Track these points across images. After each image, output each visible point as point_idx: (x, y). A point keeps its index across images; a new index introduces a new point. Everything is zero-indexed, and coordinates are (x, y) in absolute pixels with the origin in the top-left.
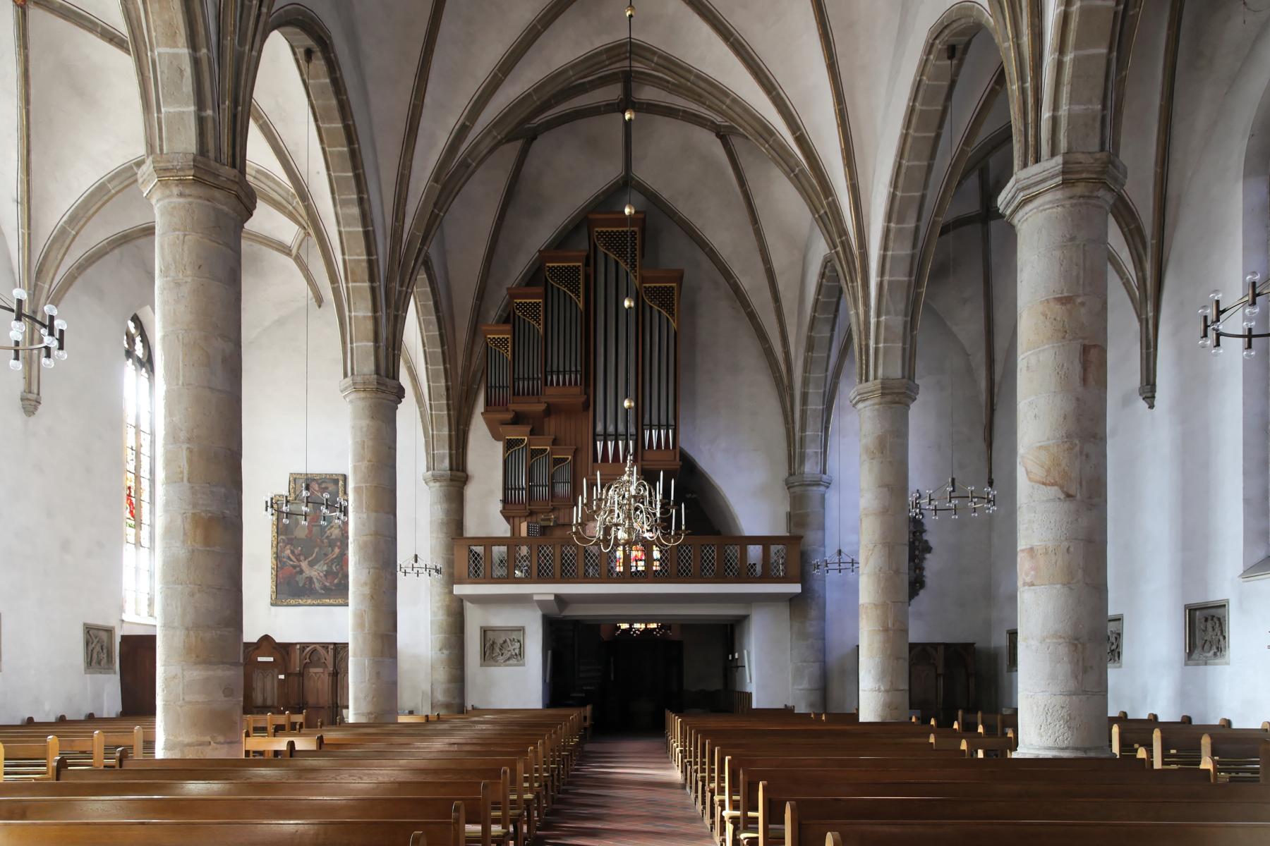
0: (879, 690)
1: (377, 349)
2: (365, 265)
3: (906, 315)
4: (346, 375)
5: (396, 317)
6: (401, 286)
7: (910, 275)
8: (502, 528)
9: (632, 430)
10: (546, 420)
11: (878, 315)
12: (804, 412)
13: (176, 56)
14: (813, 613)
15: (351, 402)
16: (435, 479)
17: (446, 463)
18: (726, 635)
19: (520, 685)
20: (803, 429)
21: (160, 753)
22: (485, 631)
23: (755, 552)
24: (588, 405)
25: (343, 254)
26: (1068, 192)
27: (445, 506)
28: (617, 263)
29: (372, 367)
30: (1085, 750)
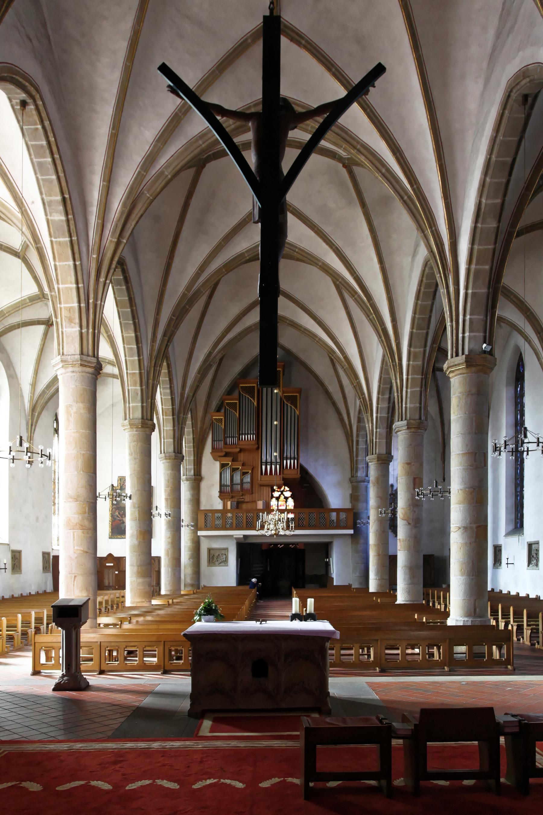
0: (376, 579)
1: (174, 441)
2: (171, 410)
3: (387, 428)
4: (161, 453)
5: (182, 427)
6: (184, 415)
7: (388, 413)
8: (218, 505)
10: (239, 454)
11: (376, 429)
12: (357, 449)
13: (136, 389)
14: (362, 541)
15: (163, 463)
17: (192, 472)
18: (324, 549)
19: (226, 575)
20: (357, 456)
22: (209, 550)
23: (334, 515)
24: (259, 448)
25: (162, 405)
26: (409, 431)
27: (192, 492)
29: (172, 449)
30: (413, 601)
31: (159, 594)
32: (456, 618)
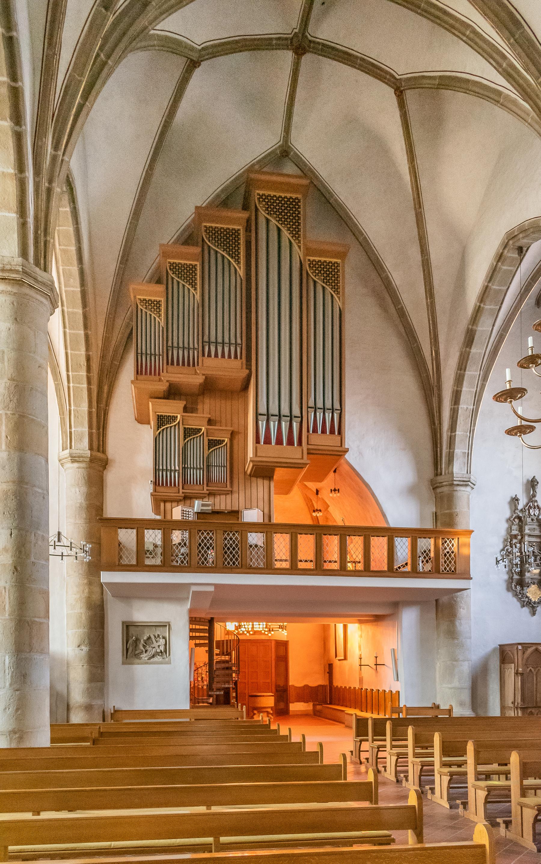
9: (296, 411)
16: (74, 459)
21: (207, 628)
27: (84, 489)
28: (279, 230)
31: (307, 255)
32: (207, 635)
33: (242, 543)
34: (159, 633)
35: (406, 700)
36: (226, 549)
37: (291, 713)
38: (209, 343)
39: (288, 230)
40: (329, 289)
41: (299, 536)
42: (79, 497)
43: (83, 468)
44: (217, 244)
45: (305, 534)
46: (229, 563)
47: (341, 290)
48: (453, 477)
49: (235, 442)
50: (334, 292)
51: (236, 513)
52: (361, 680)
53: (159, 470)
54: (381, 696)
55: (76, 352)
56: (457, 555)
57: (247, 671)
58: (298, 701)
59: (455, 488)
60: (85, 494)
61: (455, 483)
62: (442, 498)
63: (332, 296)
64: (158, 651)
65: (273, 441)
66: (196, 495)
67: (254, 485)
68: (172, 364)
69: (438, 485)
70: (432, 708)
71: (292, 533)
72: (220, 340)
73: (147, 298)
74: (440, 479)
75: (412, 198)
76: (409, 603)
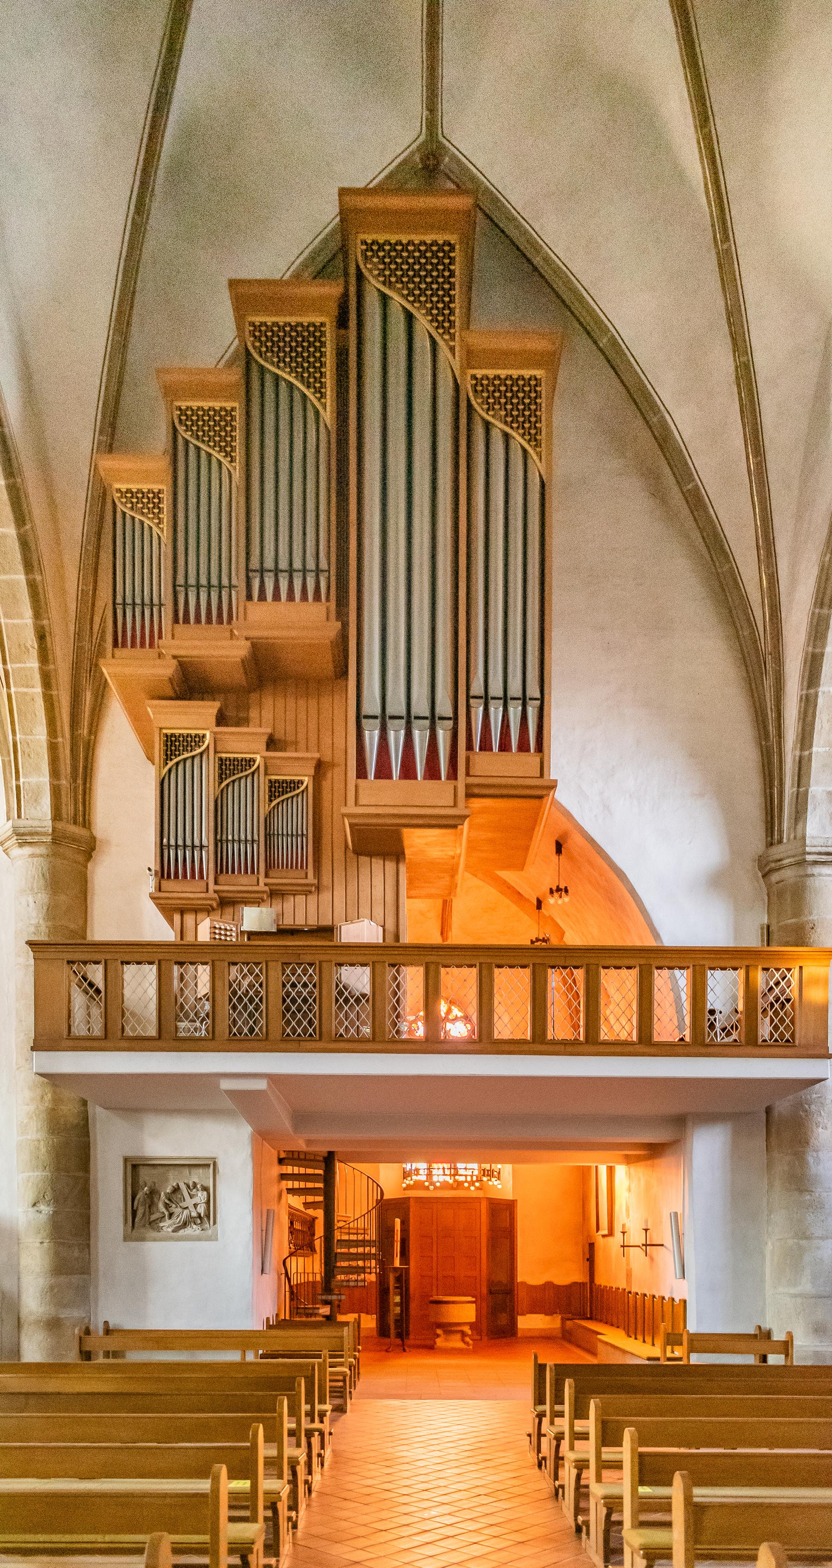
9: (444, 707)
21: (321, 1172)
22: (134, 1167)
27: (43, 898)
32: (321, 1185)
33: (320, 989)
34: (196, 1181)
35: (699, 1320)
36: (288, 1001)
37: (519, 1335)
38: (262, 571)
39: (429, 312)
40: (518, 439)
41: (443, 971)
42: (34, 914)
43: (41, 856)
44: (276, 360)
45: (458, 967)
46: (294, 1030)
47: (543, 437)
48: (804, 845)
49: (326, 785)
50: (529, 441)
51: (327, 931)
52: (629, 1275)
53: (169, 846)
54: (658, 1307)
55: (15, 621)
56: (797, 1004)
57: (434, 1255)
58: (532, 1312)
59: (811, 870)
60: (45, 908)
61: (809, 858)
62: (780, 895)
63: (525, 451)
64: (194, 1214)
65: (396, 771)
66: (245, 895)
67: (365, 871)
68: (186, 620)
69: (773, 865)
70: (755, 1336)
71: (427, 963)
72: (283, 564)
73: (134, 487)
74: (777, 852)
75: (709, 223)
76: (709, 1118)
